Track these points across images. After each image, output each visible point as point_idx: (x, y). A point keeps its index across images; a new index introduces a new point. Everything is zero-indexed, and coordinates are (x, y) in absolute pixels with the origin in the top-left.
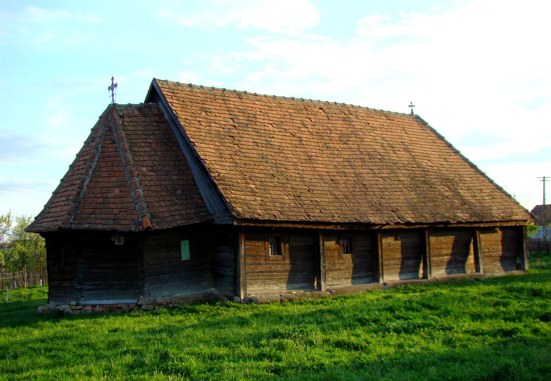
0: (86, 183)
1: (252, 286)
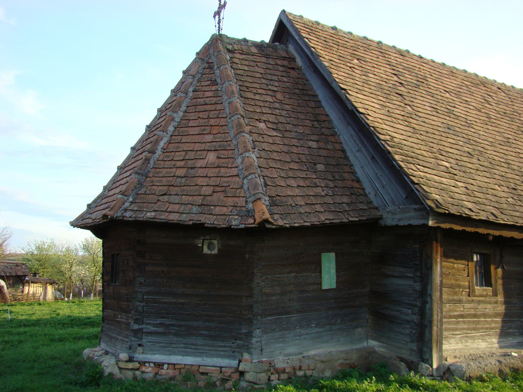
0: (162, 144)
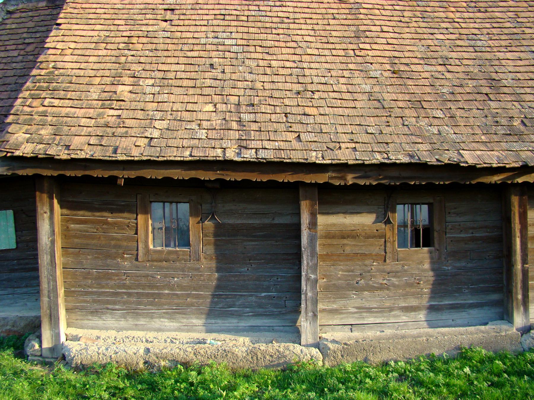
1: (97, 318)
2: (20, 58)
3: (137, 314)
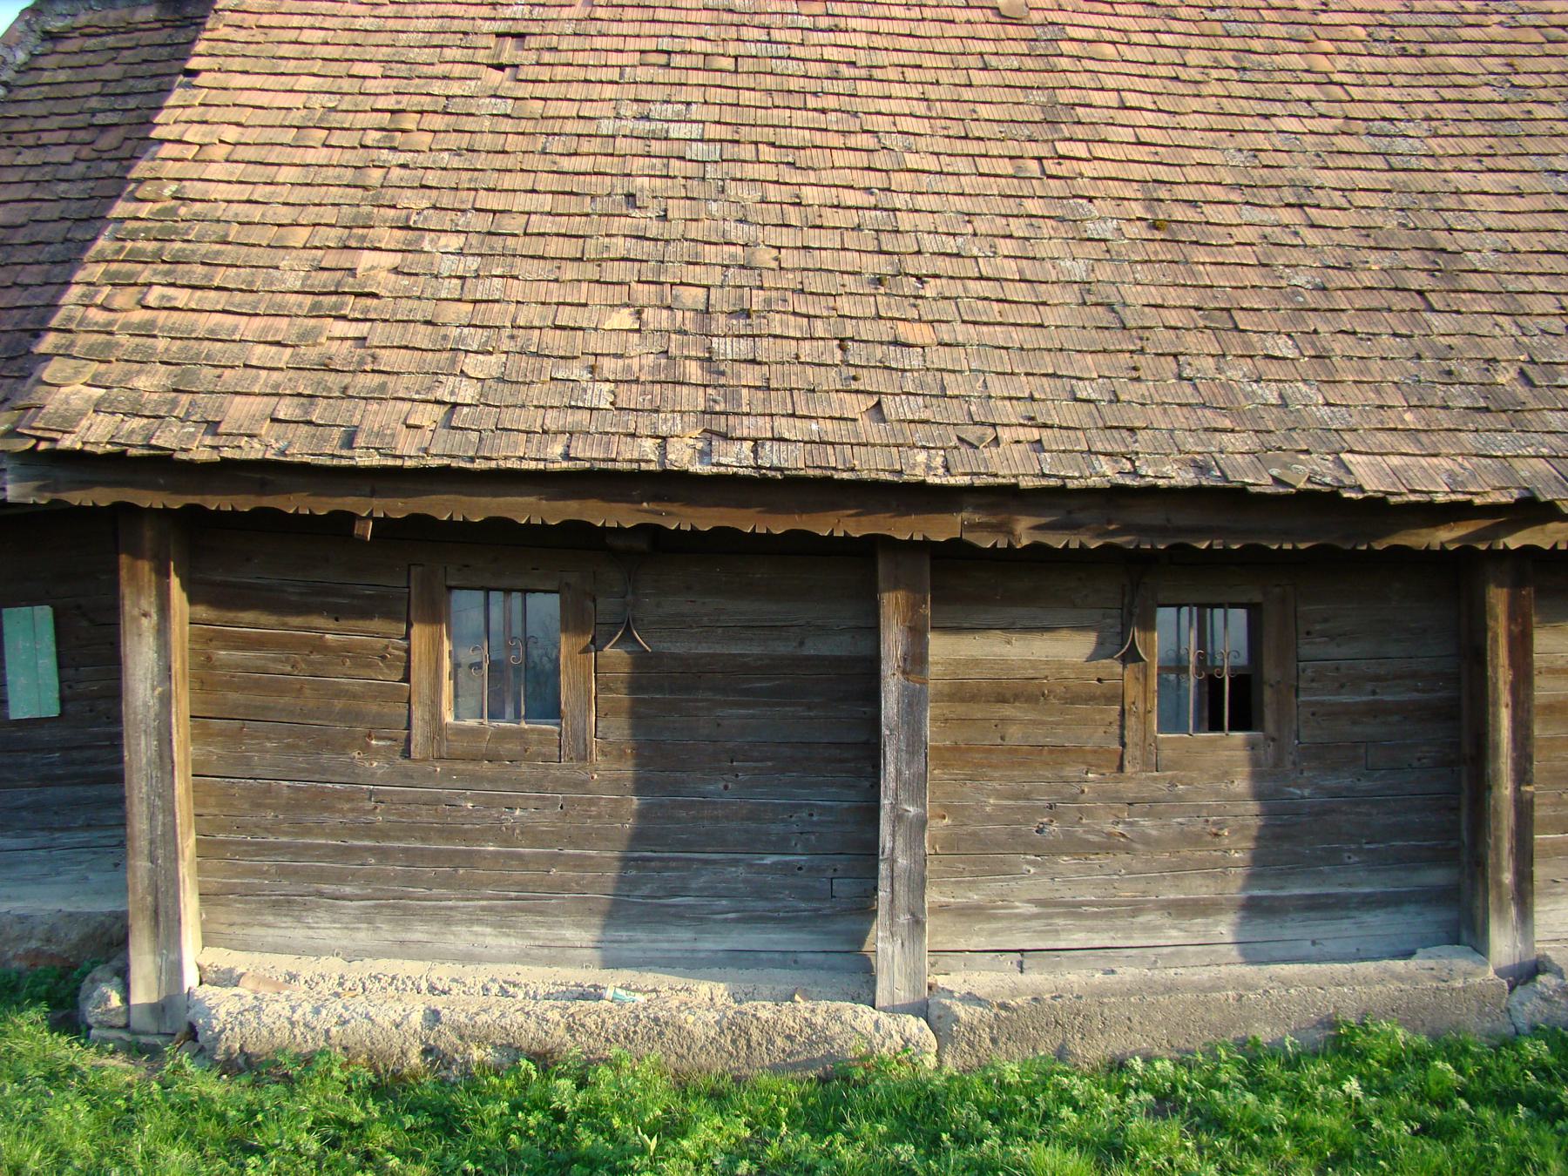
1: (288, 921)
2: (80, 168)
3: (405, 909)
